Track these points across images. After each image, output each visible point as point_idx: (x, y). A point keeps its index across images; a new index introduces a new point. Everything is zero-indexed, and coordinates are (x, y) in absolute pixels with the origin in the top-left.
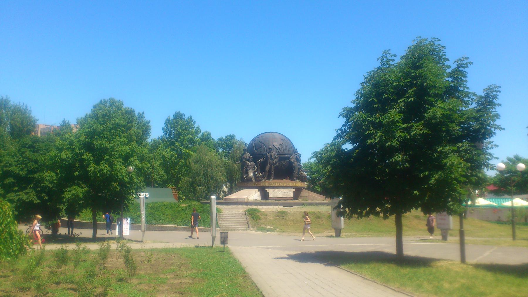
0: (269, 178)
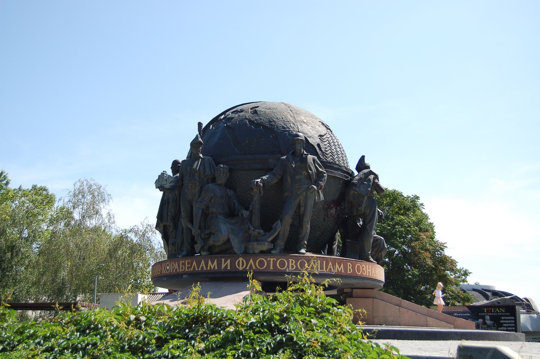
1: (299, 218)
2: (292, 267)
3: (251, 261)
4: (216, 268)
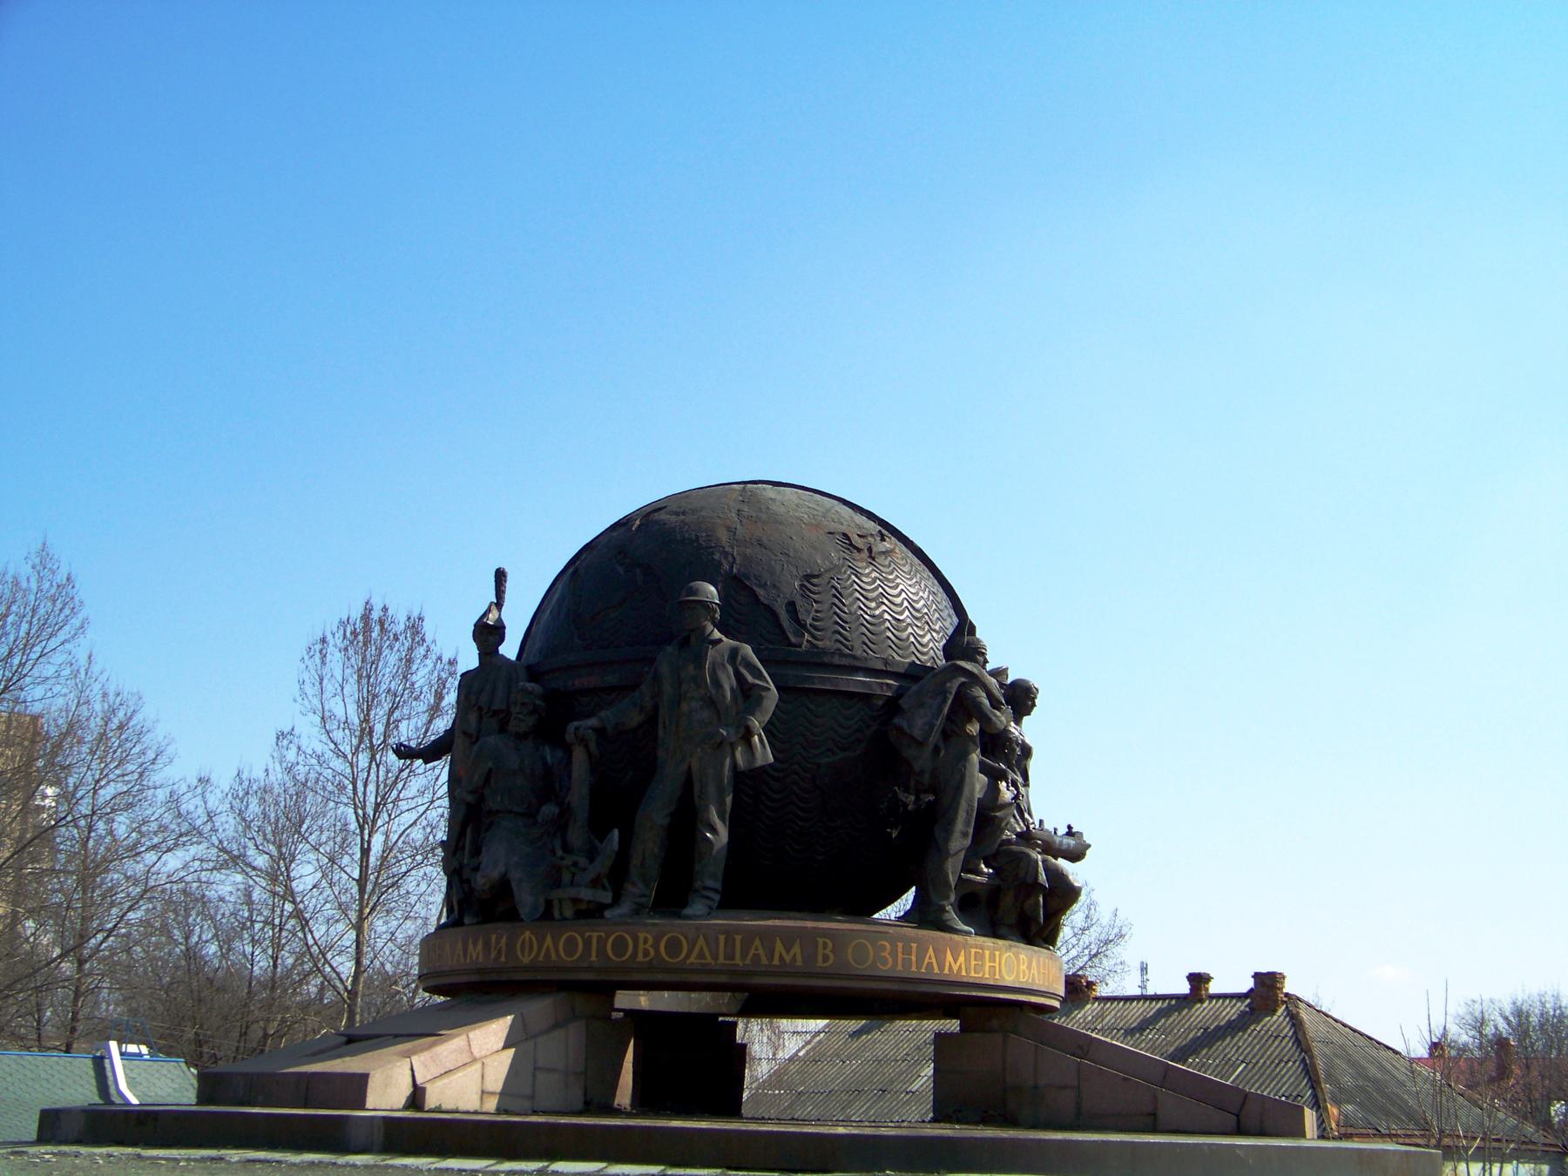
0: (672, 897)
1: (686, 820)
2: (646, 953)
3: (549, 940)
4: (799, 963)
